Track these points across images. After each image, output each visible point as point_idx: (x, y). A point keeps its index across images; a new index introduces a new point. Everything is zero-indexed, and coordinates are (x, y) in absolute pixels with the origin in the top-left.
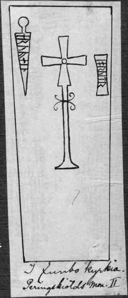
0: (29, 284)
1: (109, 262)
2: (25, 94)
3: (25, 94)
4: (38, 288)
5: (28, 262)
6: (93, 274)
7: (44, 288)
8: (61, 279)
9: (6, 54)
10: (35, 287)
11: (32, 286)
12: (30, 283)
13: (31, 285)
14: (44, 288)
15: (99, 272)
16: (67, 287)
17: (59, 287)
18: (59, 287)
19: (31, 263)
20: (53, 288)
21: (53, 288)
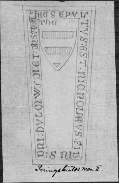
0: (40, 168)
1: (37, 152)
2: (53, 176)
3: (53, 176)
4: (47, 171)
5: (85, 15)
6: (67, 57)
7: (51, 171)
8: (54, 176)
9: (116, 145)
10: (44, 170)
11: (42, 169)
12: (41, 167)
13: (41, 168)
14: (51, 171)
15: (77, 143)
16: (70, 170)
17: (64, 170)
18: (64, 170)
19: (61, 66)
20: (59, 171)
21: (59, 171)
